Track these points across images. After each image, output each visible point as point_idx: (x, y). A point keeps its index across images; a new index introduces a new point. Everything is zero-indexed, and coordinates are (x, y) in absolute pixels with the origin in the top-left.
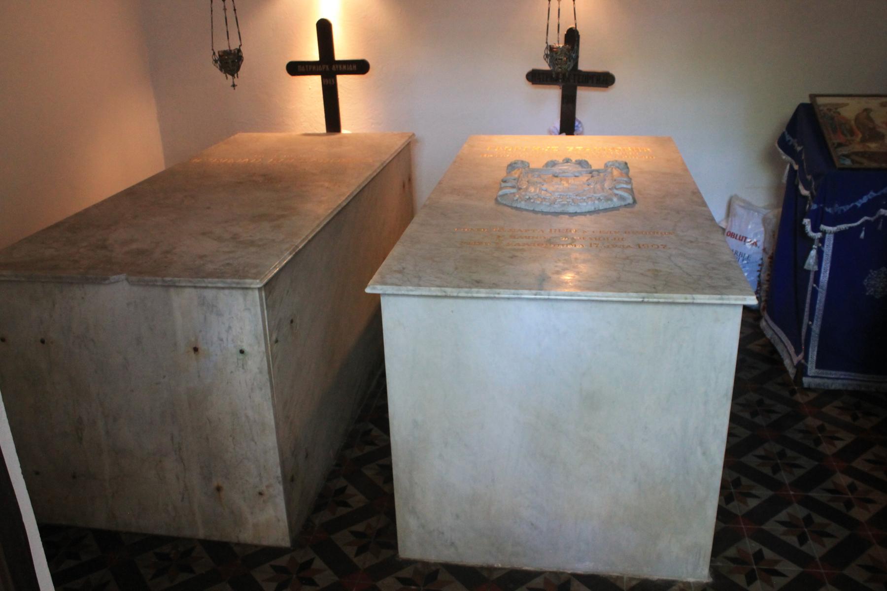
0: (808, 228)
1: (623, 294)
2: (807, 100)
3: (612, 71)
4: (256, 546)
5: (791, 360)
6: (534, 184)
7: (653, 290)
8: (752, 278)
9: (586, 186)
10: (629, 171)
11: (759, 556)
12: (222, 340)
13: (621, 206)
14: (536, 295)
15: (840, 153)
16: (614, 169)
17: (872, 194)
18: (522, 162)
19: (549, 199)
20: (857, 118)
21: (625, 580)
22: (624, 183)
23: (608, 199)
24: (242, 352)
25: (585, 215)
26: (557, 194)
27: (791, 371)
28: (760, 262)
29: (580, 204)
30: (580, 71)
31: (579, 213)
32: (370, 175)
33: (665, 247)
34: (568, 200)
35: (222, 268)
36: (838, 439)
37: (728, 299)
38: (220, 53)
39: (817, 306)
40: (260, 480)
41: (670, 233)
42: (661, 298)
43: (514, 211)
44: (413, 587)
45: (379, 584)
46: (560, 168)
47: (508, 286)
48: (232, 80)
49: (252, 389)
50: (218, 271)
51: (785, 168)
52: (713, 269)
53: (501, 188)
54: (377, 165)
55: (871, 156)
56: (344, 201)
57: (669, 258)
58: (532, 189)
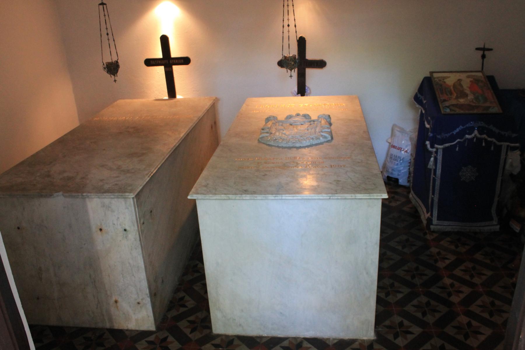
0: (429, 146)
1: (320, 195)
2: (428, 75)
3: (325, 59)
4: (137, 331)
5: (425, 216)
6: (279, 130)
7: (335, 192)
8: (406, 170)
9: (306, 131)
10: (331, 120)
11: (401, 324)
12: (114, 224)
13: (325, 142)
14: (275, 197)
15: (444, 105)
16: (322, 119)
17: (461, 127)
18: (273, 117)
19: (286, 139)
20: (454, 85)
21: (331, 340)
22: (326, 129)
23: (317, 138)
24: (125, 230)
25: (305, 148)
26: (291, 136)
27: (425, 222)
28: (410, 161)
29: (302, 142)
30: (307, 60)
31: (302, 147)
32: (192, 126)
33: (344, 166)
34: (296, 140)
35: (113, 187)
36: (447, 259)
37: (373, 196)
38: (107, 64)
39: (436, 187)
40: (138, 296)
41: (348, 158)
42: (339, 197)
43: (267, 147)
44: (220, 349)
45: (203, 348)
46: (294, 119)
47: (261, 193)
48: (114, 78)
49: (131, 249)
50: (111, 189)
51: (419, 111)
52: (368, 178)
53: (261, 133)
54: (196, 119)
55: (461, 106)
56: (177, 143)
57: (346, 173)
58: (277, 134)
